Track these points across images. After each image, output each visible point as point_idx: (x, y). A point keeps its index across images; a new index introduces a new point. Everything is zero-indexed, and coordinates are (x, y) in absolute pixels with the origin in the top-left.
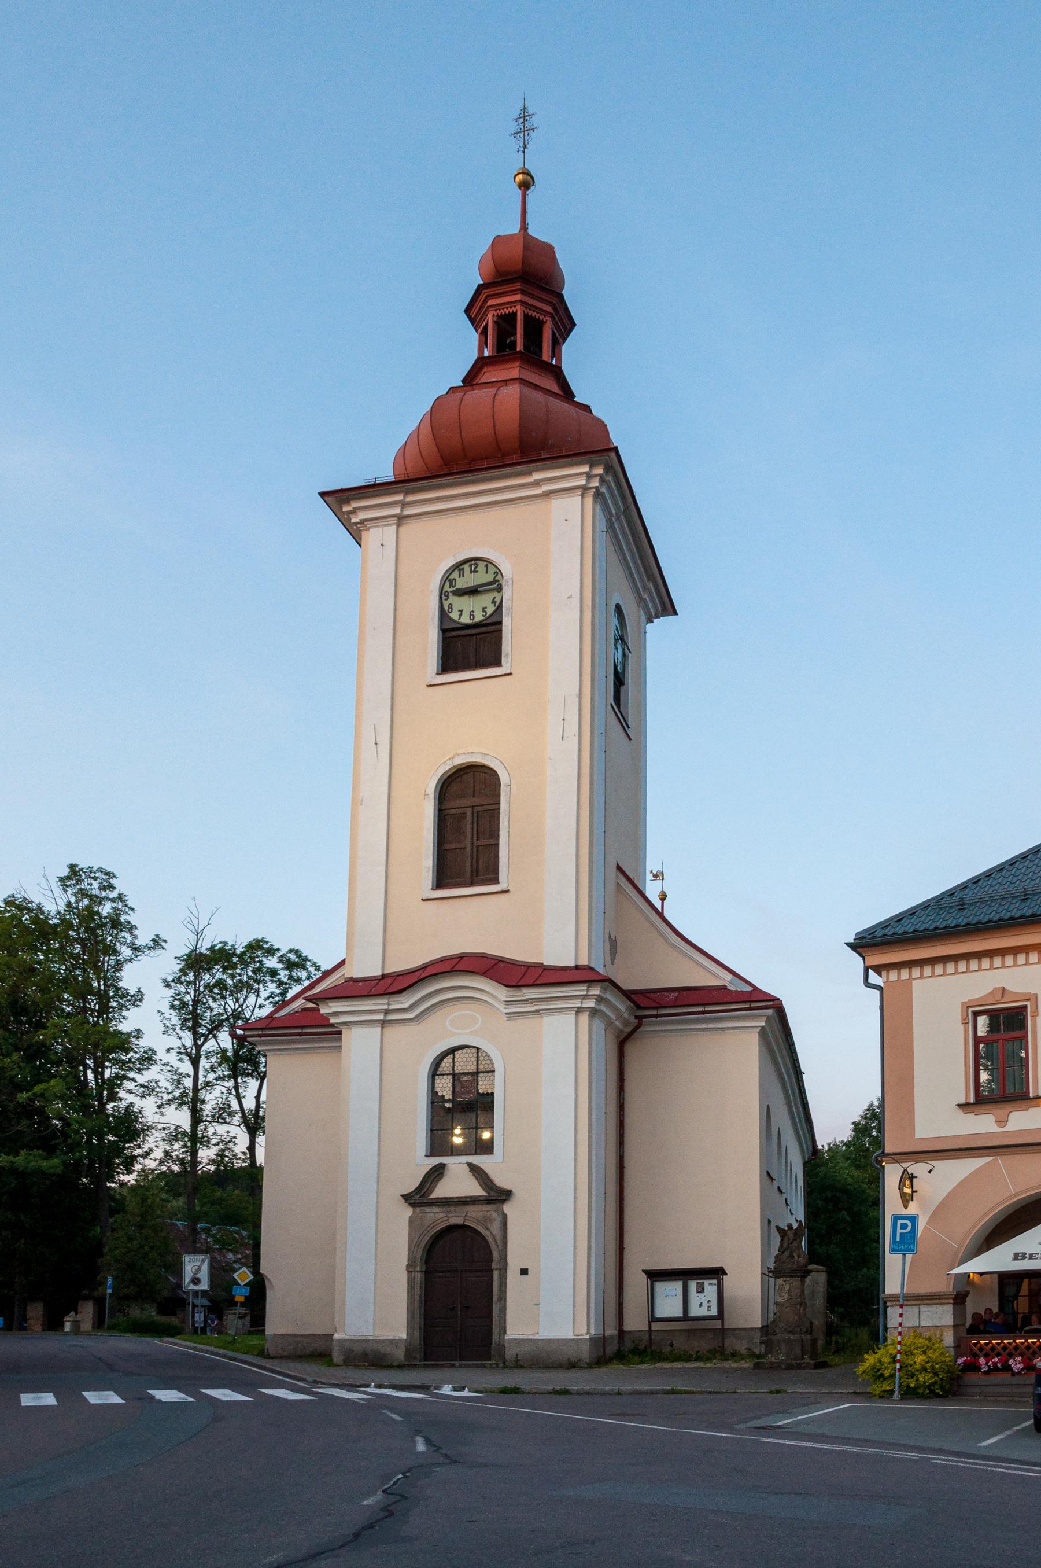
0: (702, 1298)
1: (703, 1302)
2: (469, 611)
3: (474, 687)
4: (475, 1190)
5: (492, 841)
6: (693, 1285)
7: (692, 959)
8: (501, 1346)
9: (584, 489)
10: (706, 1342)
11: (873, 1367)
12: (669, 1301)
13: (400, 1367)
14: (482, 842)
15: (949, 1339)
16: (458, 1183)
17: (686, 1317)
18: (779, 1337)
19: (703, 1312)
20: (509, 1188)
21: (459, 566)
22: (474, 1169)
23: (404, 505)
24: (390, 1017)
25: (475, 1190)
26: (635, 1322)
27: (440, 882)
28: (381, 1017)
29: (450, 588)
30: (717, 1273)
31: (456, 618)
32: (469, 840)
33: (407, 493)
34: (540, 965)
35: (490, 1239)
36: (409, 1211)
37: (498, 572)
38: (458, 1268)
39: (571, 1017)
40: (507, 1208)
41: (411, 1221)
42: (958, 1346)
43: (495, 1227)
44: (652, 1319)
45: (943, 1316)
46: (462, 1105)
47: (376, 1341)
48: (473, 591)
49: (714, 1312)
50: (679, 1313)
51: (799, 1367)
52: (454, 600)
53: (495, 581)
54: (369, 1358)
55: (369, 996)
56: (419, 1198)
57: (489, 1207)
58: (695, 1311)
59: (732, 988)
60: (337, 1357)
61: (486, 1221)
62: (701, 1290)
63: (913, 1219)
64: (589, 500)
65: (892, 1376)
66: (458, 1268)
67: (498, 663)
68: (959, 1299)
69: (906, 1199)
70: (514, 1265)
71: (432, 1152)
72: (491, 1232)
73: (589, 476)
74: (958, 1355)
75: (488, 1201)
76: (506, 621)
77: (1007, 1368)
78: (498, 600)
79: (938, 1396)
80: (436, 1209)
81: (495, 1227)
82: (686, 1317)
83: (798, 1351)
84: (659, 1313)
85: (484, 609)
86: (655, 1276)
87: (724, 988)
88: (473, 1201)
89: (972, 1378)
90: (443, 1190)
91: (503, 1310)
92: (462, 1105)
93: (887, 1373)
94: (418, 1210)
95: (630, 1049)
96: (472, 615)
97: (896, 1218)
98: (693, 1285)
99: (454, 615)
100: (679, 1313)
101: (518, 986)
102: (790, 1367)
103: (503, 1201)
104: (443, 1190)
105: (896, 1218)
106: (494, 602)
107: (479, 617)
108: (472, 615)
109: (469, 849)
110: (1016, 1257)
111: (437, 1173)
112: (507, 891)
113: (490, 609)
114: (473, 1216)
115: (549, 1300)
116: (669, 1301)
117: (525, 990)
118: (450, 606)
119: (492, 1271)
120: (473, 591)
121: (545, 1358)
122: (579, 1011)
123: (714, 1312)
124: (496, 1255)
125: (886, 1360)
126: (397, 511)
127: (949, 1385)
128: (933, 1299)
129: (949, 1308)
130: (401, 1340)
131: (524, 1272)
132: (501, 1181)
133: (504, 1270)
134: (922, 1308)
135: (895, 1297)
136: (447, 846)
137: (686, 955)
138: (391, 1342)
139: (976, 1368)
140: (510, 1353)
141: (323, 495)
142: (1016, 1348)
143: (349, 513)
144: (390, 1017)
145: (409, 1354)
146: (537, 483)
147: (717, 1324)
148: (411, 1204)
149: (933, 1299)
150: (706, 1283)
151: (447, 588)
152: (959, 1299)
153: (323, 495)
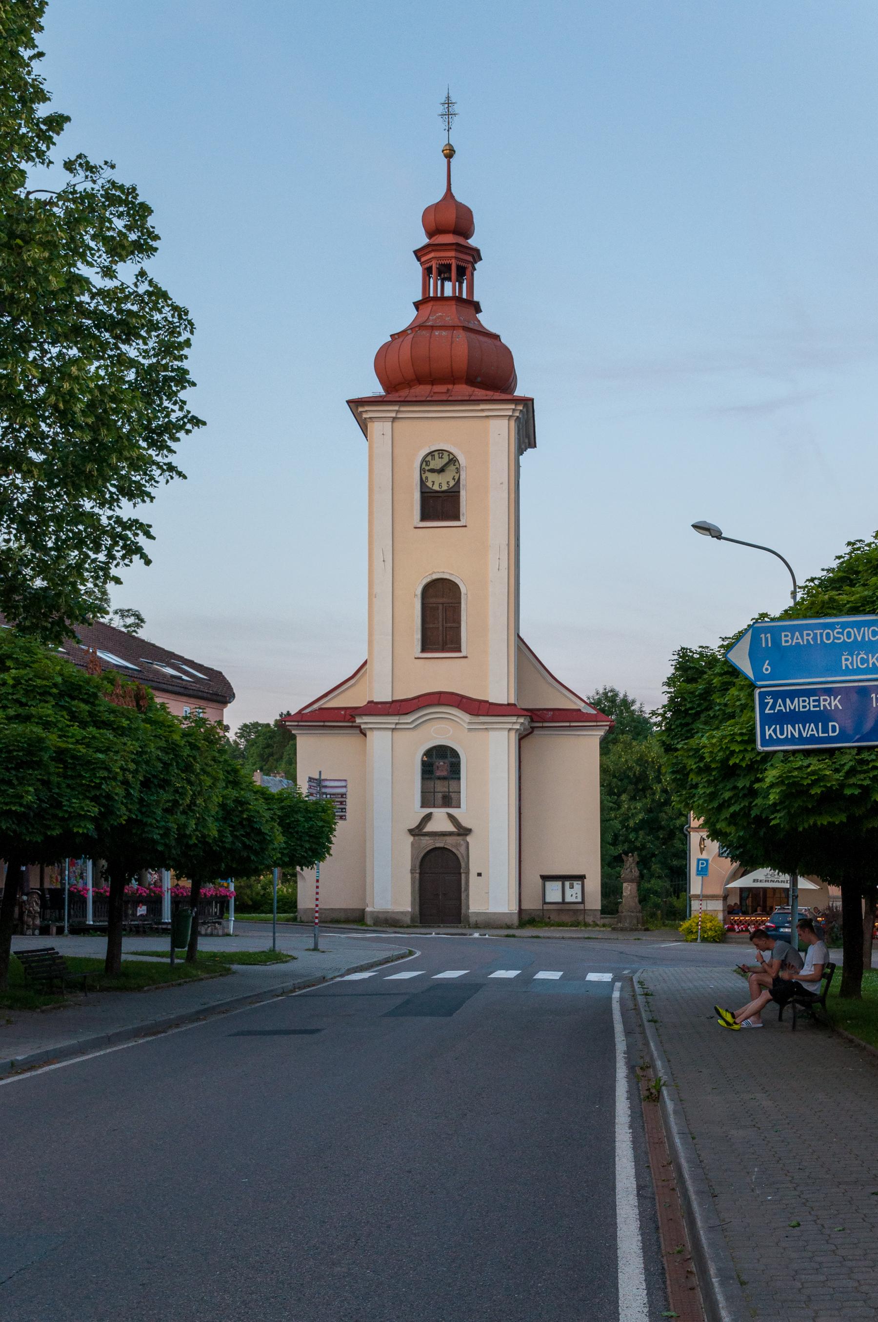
0: (573, 891)
1: (573, 894)
2: (439, 483)
3: (441, 533)
4: (450, 827)
5: (454, 625)
6: (567, 884)
7: (561, 693)
8: (467, 916)
9: (510, 416)
10: (568, 916)
11: (688, 928)
12: (554, 892)
13: (408, 927)
14: (449, 625)
15: (720, 916)
16: (440, 822)
17: (564, 902)
18: (625, 914)
19: (573, 900)
20: (469, 827)
21: (431, 453)
22: (451, 817)
23: (397, 412)
24: (398, 727)
25: (450, 827)
26: (532, 904)
27: (426, 646)
28: (393, 726)
29: (425, 466)
30: (581, 878)
31: (430, 486)
32: (441, 623)
33: (400, 406)
34: (487, 702)
35: (459, 856)
36: (411, 839)
37: (450, 453)
38: (440, 875)
39: (506, 733)
40: (469, 839)
41: (412, 844)
42: (725, 921)
43: (463, 849)
44: (545, 903)
45: (718, 906)
46: (441, 770)
47: (394, 913)
48: (442, 470)
49: (579, 900)
50: (560, 900)
51: (636, 930)
52: (428, 474)
53: (450, 461)
54: (388, 922)
55: (388, 714)
56: (417, 832)
57: (458, 838)
58: (568, 899)
59: (584, 711)
60: (369, 921)
61: (457, 845)
62: (572, 887)
63: (707, 861)
64: (513, 423)
65: (697, 932)
66: (440, 875)
67: (457, 517)
68: (725, 898)
69: (702, 850)
70: (473, 870)
71: (424, 805)
72: (460, 852)
73: (514, 410)
74: (725, 923)
75: (459, 835)
76: (463, 493)
77: (747, 930)
78: (457, 478)
79: (716, 942)
80: (427, 838)
81: (463, 849)
82: (564, 902)
83: (635, 922)
84: (548, 900)
85: (448, 482)
86: (545, 878)
87: (579, 710)
88: (450, 834)
89: (731, 934)
90: (430, 827)
91: (468, 896)
92: (441, 770)
93: (694, 931)
94: (417, 838)
95: (522, 742)
96: (440, 485)
97: (699, 860)
98: (567, 884)
99: (429, 484)
100: (560, 900)
101: (478, 715)
102: (632, 930)
103: (467, 835)
104: (430, 827)
105: (699, 860)
106: (454, 479)
107: (445, 488)
108: (440, 485)
109: (441, 628)
110: (754, 881)
111: (428, 818)
112: (466, 657)
113: (452, 483)
114: (449, 843)
115: (493, 890)
116: (554, 892)
117: (481, 718)
118: (427, 478)
119: (460, 874)
120: (442, 470)
121: (489, 923)
122: (510, 730)
123: (579, 900)
124: (463, 865)
125: (694, 924)
126: (393, 415)
127: (721, 937)
128: (713, 897)
129: (721, 902)
130: (408, 912)
131: (479, 875)
132: (465, 823)
133: (467, 873)
134: (708, 902)
135: (697, 897)
136: (427, 626)
137: (558, 690)
138: (402, 913)
139: (734, 930)
140: (473, 920)
141: (348, 402)
142: (752, 921)
143: (361, 412)
144: (398, 727)
145: (413, 920)
146: (482, 410)
147: (581, 907)
148: (413, 835)
149: (713, 897)
150: (575, 883)
151: (424, 466)
152: (725, 898)
153: (348, 402)
